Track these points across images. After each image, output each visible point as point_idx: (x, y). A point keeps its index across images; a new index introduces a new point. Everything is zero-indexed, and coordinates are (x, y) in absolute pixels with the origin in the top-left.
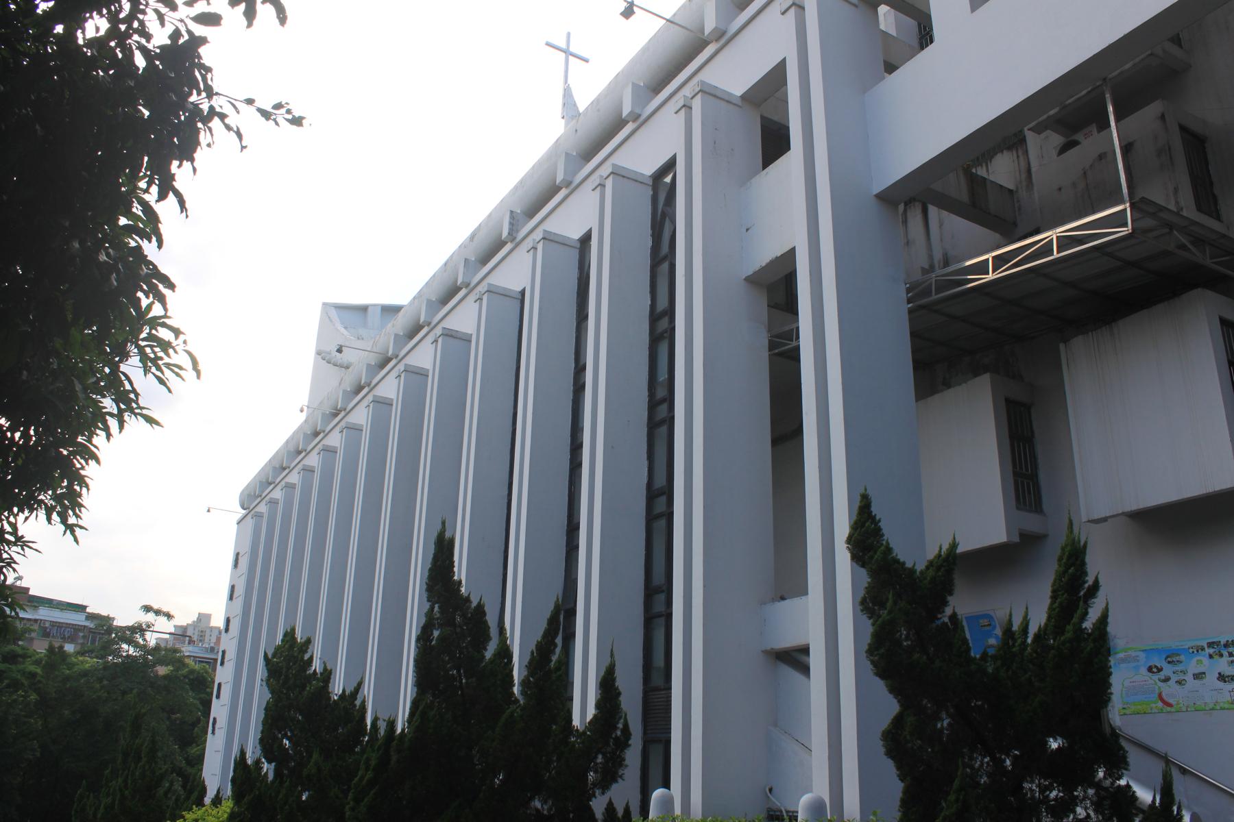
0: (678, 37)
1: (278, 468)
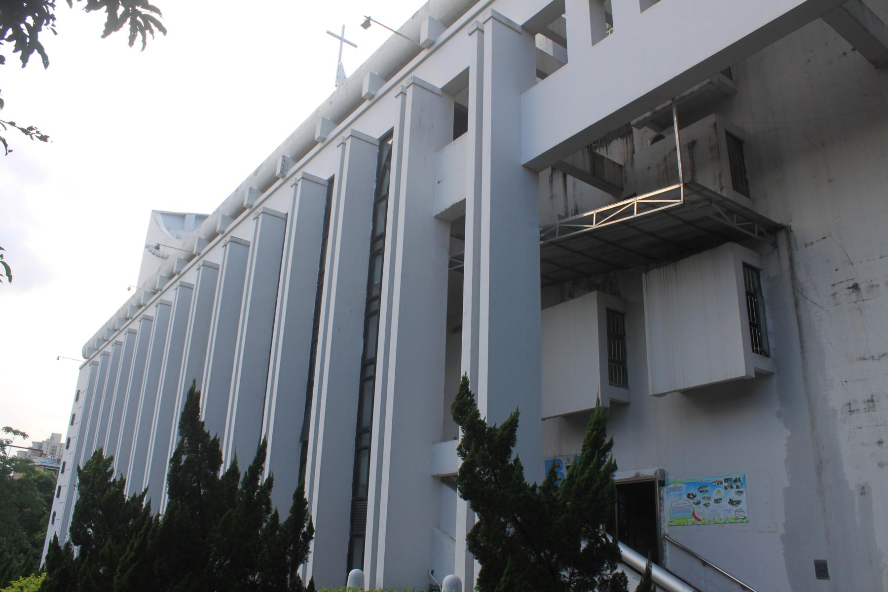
0: (403, 45)
1: (111, 330)
